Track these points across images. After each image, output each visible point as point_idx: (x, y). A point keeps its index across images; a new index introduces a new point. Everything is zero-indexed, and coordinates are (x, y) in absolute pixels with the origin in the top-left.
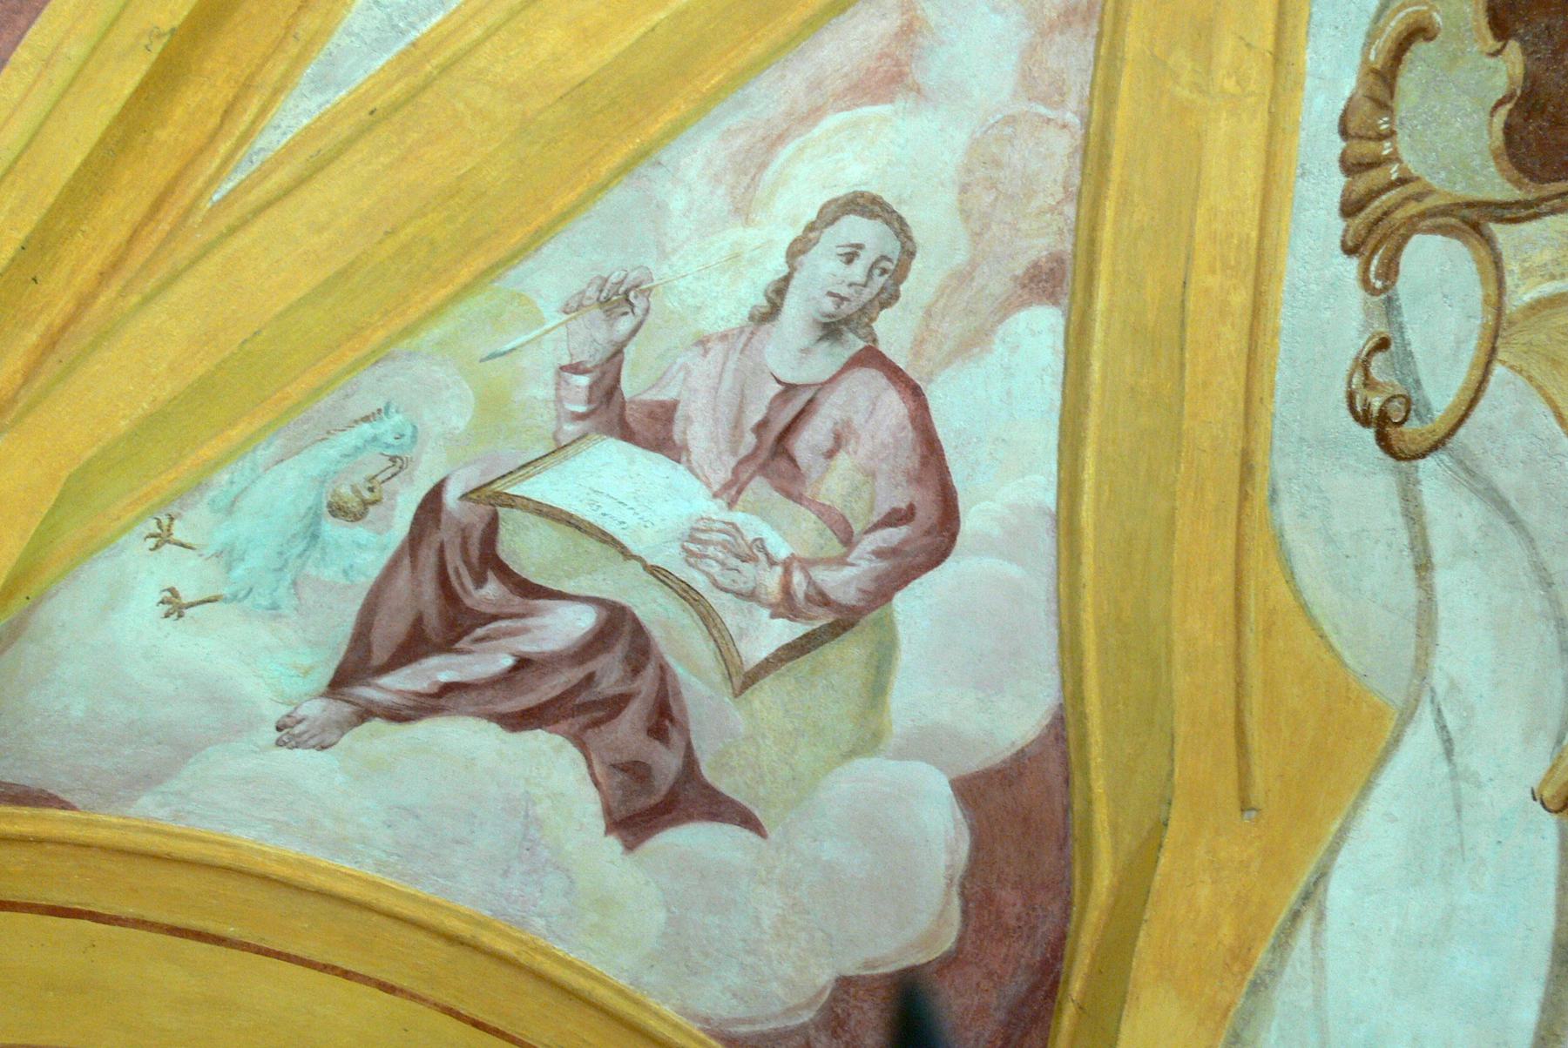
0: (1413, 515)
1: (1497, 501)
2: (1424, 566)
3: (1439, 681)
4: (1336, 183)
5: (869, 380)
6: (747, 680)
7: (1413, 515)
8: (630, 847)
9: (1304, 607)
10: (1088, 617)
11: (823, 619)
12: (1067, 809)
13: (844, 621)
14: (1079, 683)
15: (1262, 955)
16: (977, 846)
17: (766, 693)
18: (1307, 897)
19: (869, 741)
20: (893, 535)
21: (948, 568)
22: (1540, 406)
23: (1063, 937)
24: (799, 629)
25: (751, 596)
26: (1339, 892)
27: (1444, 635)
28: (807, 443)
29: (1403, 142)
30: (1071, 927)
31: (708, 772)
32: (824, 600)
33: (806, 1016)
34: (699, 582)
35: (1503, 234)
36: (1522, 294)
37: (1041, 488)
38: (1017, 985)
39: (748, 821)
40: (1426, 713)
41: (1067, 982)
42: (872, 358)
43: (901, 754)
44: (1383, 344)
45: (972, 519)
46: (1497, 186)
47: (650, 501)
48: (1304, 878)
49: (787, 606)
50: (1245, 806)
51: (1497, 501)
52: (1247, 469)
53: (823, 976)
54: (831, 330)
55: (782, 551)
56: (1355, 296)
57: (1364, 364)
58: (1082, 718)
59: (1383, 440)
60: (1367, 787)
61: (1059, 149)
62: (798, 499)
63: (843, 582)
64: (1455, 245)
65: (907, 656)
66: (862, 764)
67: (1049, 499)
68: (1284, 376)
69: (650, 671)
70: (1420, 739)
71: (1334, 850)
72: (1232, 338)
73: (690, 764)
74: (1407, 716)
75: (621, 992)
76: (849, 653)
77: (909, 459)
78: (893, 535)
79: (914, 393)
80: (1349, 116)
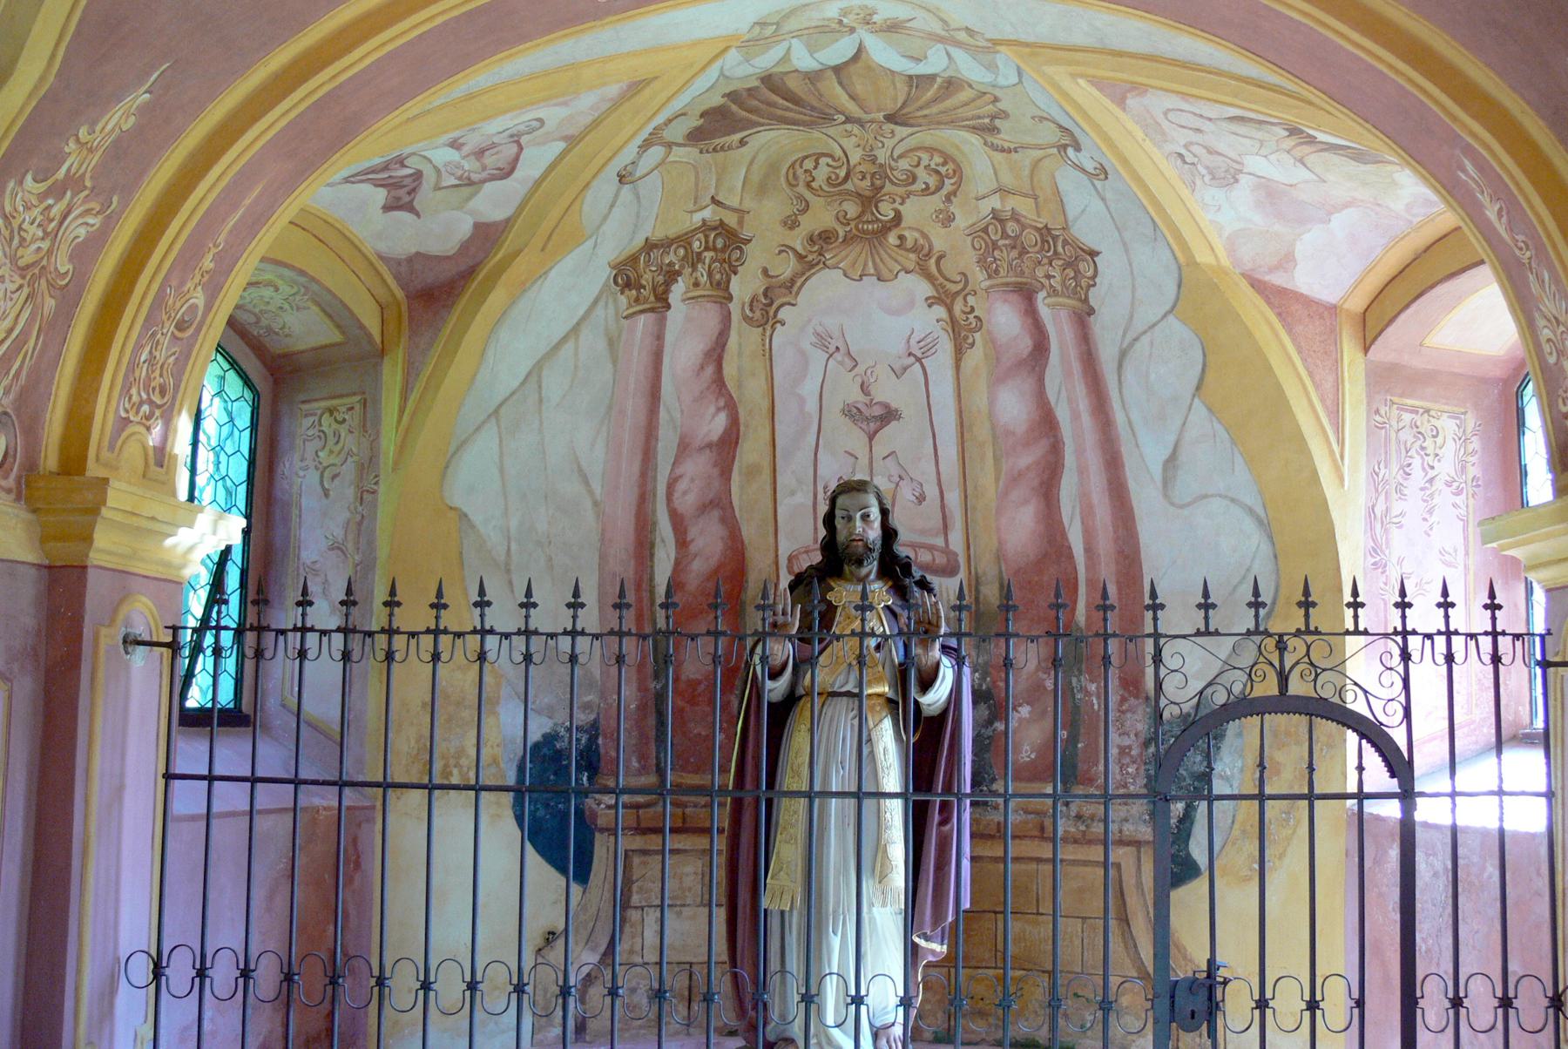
0: (617, 196)
1: (638, 198)
2: (612, 206)
3: (601, 231)
4: (646, 136)
5: (515, 145)
6: (438, 188)
7: (617, 196)
8: (384, 212)
9: (580, 211)
10: (532, 202)
11: (466, 182)
12: (500, 237)
13: (471, 183)
14: (520, 214)
15: (528, 285)
16: (470, 237)
17: (440, 194)
18: (545, 273)
19: (460, 208)
20: (495, 172)
21: (504, 181)
22: (660, 180)
23: (481, 262)
24: (457, 182)
25: (453, 174)
26: (553, 273)
27: (609, 221)
28: (487, 153)
29: (665, 132)
30: (486, 261)
31: (415, 203)
32: (469, 179)
33: (403, 257)
34: (443, 170)
35: (674, 148)
36: (671, 158)
37: (537, 173)
38: (463, 268)
39: (418, 215)
40: (594, 237)
41: (478, 274)
42: (518, 142)
43: (465, 213)
44: (633, 163)
45: (517, 174)
46: (681, 141)
47: (944, 988)
48: (547, 268)
49: (460, 178)
50: (543, 250)
51: (638, 198)
52: (587, 185)
53: (413, 250)
54: (512, 136)
55: (467, 167)
56: (635, 154)
57: (626, 166)
58: (516, 221)
59: (620, 181)
60: (571, 252)
61: (590, 119)
62: (478, 160)
63: (475, 177)
64: (663, 149)
65: (481, 195)
66: (455, 212)
67: (537, 177)
68: (608, 168)
69: (416, 183)
70: (590, 243)
71: (556, 264)
72: (602, 161)
73: (412, 201)
74: (590, 237)
75: (360, 240)
76: (466, 191)
77: (513, 156)
78: (495, 172)
79: (521, 148)
80: (716, 472)
